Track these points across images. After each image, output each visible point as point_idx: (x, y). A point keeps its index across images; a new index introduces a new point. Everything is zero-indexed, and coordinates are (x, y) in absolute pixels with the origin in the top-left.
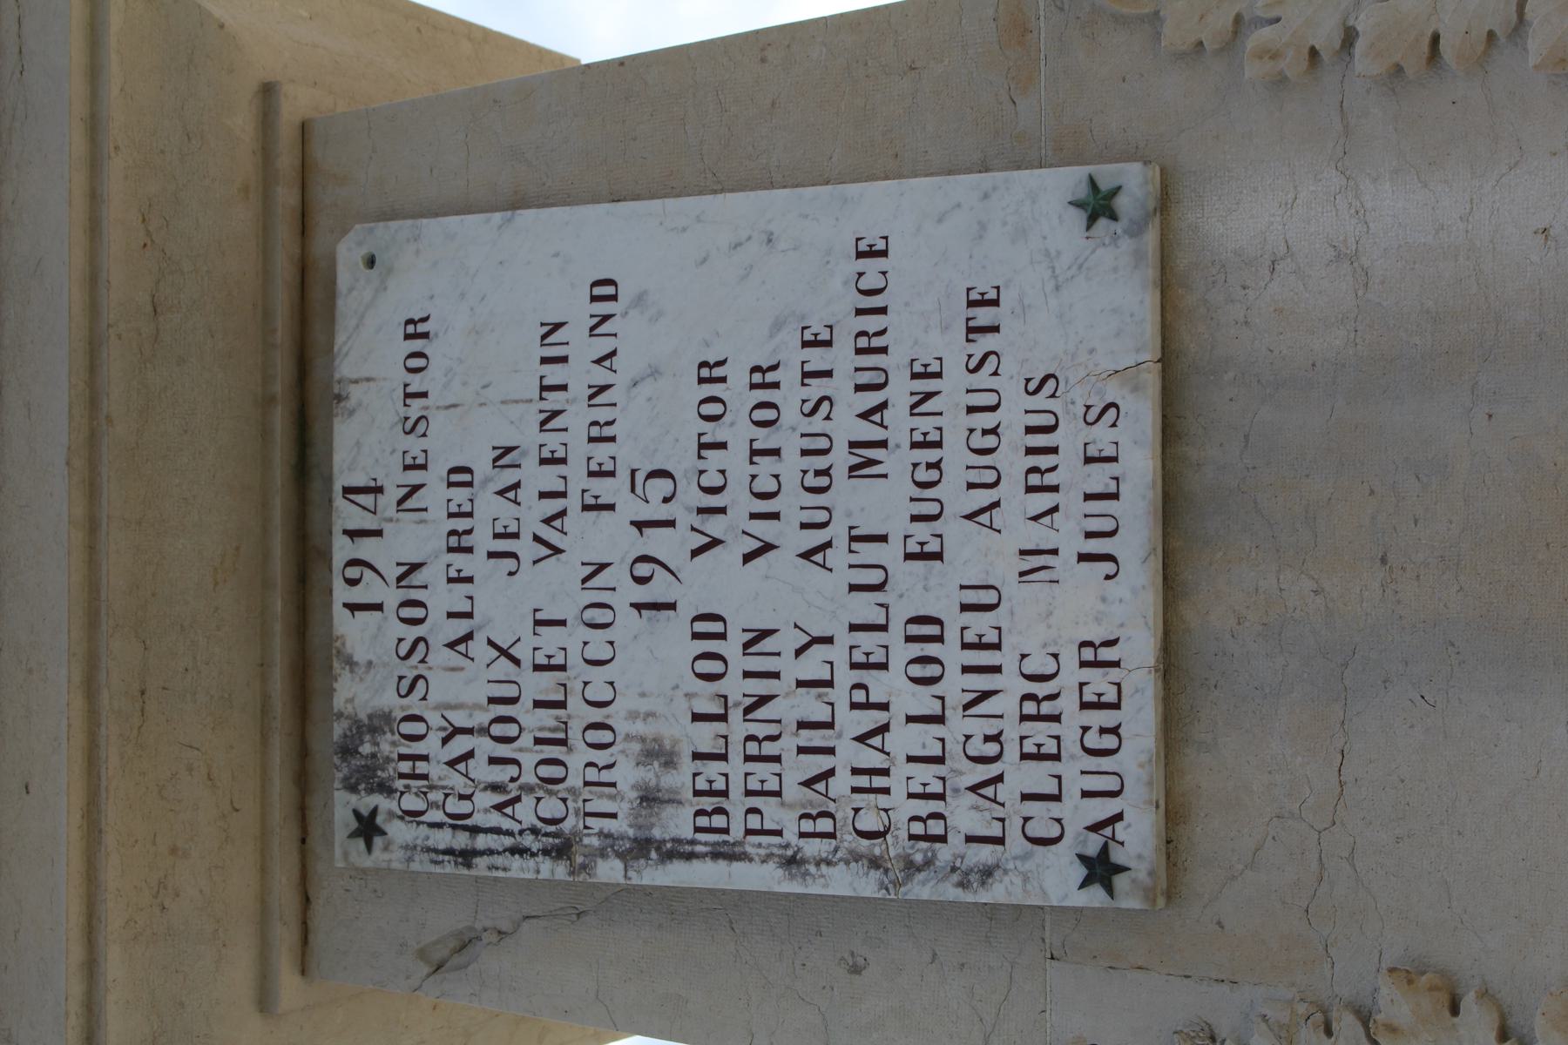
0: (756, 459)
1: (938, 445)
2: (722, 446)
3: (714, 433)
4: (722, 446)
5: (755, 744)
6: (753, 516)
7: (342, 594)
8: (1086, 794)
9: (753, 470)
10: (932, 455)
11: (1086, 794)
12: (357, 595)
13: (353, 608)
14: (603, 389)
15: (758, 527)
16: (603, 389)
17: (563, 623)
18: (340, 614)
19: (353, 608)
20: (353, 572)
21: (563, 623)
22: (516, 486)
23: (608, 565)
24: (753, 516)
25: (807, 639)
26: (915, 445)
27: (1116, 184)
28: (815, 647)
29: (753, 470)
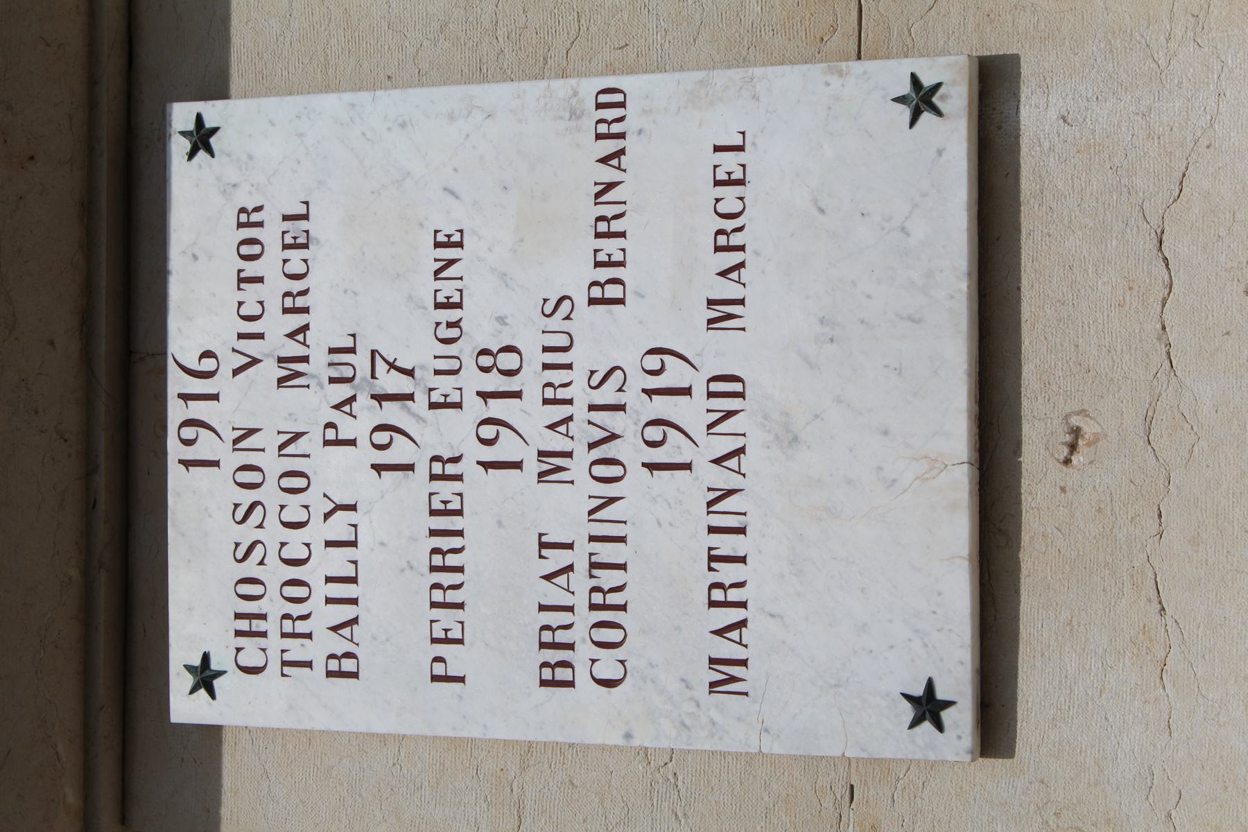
0: (243, 286)
1: (459, 306)
2: (260, 280)
3: (251, 269)
4: (260, 280)
5: (336, 661)
6: (241, 336)
7: (175, 450)
8: (329, 601)
9: (240, 296)
10: (453, 315)
11: (329, 601)
12: (190, 453)
13: (187, 464)
14: (610, 186)
15: (244, 345)
16: (610, 186)
17: (329, 544)
18: (175, 473)
19: (187, 464)
20: (188, 433)
21: (329, 544)
22: (305, 328)
23: (303, 434)
24: (241, 336)
25: (333, 506)
26: (438, 306)
27: (216, 153)
28: (339, 513)
29: (240, 296)
